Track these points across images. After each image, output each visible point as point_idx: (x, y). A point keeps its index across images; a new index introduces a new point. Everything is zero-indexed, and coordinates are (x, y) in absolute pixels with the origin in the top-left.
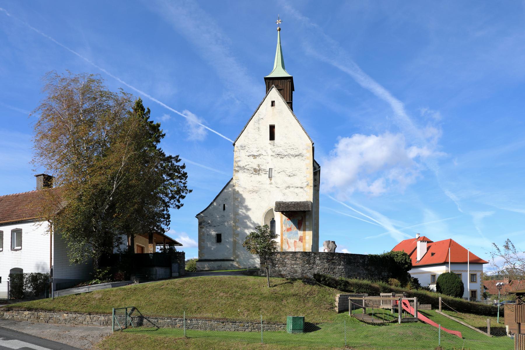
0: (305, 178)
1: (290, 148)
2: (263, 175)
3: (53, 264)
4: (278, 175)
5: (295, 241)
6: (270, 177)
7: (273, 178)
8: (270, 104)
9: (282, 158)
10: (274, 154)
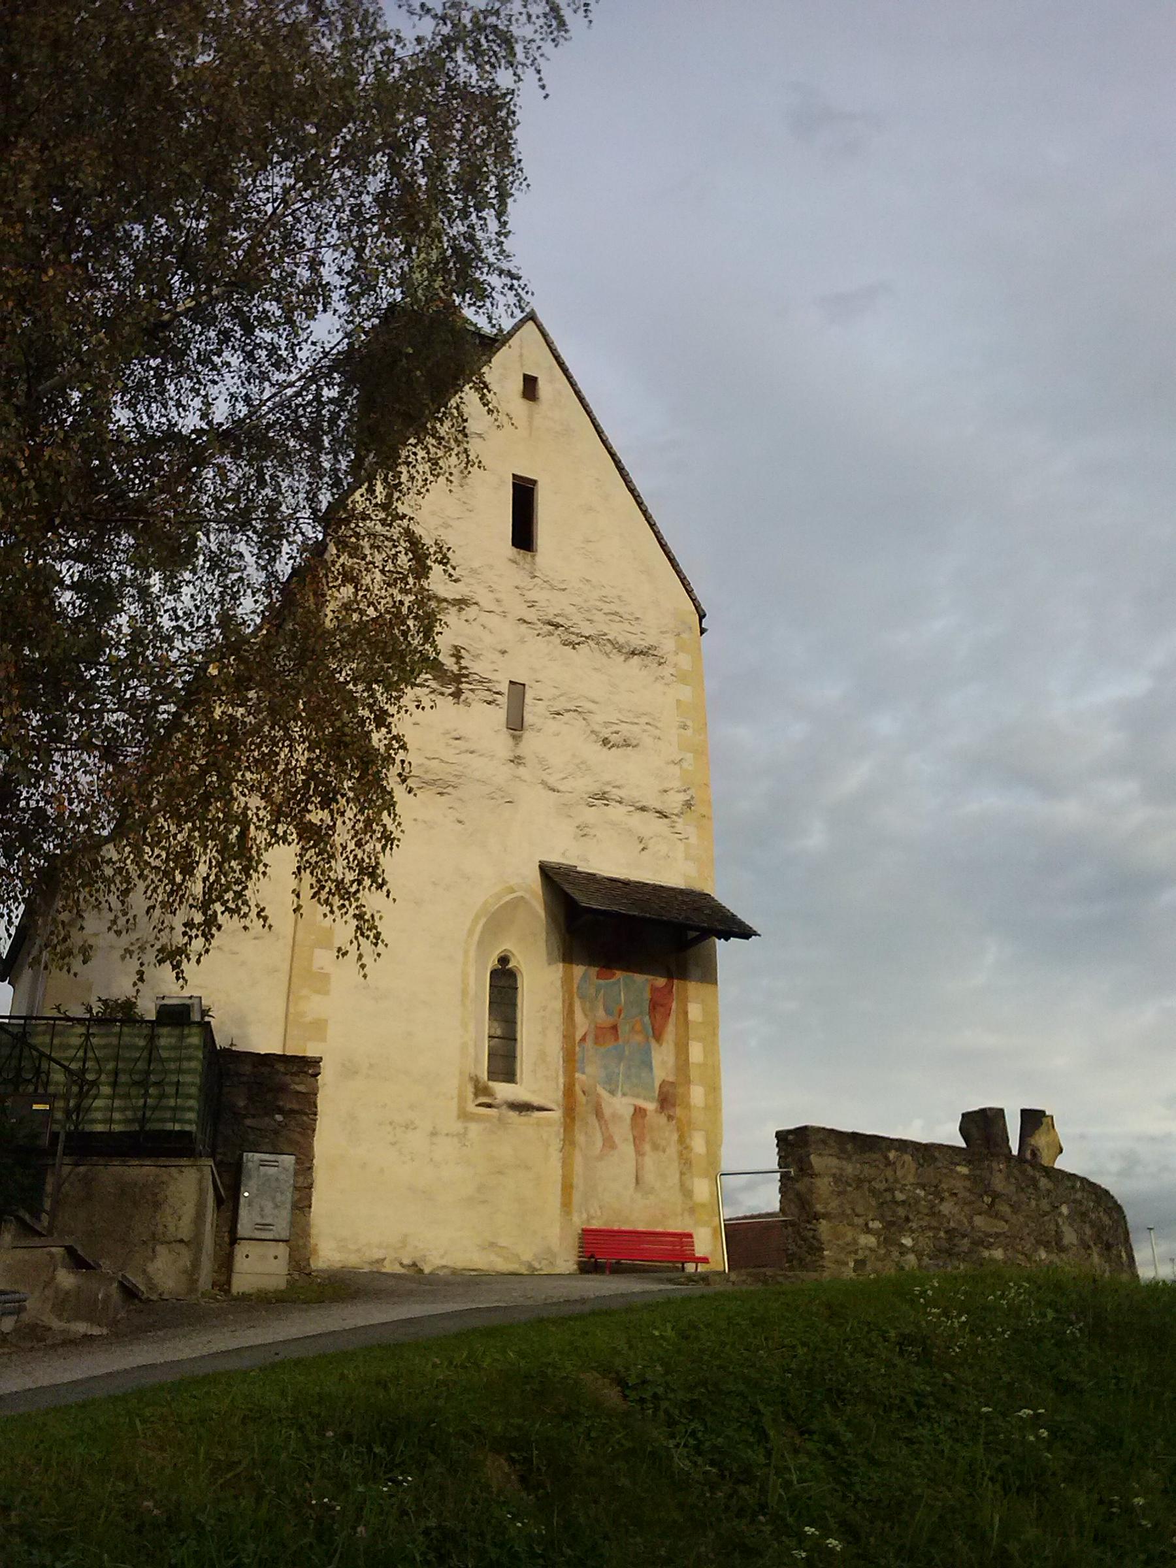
0: (676, 770)
1: (607, 608)
2: (479, 708)
3: (467, 1273)
4: (553, 725)
5: (639, 1112)
6: (516, 725)
7: (527, 735)
8: (519, 385)
10: (531, 615)
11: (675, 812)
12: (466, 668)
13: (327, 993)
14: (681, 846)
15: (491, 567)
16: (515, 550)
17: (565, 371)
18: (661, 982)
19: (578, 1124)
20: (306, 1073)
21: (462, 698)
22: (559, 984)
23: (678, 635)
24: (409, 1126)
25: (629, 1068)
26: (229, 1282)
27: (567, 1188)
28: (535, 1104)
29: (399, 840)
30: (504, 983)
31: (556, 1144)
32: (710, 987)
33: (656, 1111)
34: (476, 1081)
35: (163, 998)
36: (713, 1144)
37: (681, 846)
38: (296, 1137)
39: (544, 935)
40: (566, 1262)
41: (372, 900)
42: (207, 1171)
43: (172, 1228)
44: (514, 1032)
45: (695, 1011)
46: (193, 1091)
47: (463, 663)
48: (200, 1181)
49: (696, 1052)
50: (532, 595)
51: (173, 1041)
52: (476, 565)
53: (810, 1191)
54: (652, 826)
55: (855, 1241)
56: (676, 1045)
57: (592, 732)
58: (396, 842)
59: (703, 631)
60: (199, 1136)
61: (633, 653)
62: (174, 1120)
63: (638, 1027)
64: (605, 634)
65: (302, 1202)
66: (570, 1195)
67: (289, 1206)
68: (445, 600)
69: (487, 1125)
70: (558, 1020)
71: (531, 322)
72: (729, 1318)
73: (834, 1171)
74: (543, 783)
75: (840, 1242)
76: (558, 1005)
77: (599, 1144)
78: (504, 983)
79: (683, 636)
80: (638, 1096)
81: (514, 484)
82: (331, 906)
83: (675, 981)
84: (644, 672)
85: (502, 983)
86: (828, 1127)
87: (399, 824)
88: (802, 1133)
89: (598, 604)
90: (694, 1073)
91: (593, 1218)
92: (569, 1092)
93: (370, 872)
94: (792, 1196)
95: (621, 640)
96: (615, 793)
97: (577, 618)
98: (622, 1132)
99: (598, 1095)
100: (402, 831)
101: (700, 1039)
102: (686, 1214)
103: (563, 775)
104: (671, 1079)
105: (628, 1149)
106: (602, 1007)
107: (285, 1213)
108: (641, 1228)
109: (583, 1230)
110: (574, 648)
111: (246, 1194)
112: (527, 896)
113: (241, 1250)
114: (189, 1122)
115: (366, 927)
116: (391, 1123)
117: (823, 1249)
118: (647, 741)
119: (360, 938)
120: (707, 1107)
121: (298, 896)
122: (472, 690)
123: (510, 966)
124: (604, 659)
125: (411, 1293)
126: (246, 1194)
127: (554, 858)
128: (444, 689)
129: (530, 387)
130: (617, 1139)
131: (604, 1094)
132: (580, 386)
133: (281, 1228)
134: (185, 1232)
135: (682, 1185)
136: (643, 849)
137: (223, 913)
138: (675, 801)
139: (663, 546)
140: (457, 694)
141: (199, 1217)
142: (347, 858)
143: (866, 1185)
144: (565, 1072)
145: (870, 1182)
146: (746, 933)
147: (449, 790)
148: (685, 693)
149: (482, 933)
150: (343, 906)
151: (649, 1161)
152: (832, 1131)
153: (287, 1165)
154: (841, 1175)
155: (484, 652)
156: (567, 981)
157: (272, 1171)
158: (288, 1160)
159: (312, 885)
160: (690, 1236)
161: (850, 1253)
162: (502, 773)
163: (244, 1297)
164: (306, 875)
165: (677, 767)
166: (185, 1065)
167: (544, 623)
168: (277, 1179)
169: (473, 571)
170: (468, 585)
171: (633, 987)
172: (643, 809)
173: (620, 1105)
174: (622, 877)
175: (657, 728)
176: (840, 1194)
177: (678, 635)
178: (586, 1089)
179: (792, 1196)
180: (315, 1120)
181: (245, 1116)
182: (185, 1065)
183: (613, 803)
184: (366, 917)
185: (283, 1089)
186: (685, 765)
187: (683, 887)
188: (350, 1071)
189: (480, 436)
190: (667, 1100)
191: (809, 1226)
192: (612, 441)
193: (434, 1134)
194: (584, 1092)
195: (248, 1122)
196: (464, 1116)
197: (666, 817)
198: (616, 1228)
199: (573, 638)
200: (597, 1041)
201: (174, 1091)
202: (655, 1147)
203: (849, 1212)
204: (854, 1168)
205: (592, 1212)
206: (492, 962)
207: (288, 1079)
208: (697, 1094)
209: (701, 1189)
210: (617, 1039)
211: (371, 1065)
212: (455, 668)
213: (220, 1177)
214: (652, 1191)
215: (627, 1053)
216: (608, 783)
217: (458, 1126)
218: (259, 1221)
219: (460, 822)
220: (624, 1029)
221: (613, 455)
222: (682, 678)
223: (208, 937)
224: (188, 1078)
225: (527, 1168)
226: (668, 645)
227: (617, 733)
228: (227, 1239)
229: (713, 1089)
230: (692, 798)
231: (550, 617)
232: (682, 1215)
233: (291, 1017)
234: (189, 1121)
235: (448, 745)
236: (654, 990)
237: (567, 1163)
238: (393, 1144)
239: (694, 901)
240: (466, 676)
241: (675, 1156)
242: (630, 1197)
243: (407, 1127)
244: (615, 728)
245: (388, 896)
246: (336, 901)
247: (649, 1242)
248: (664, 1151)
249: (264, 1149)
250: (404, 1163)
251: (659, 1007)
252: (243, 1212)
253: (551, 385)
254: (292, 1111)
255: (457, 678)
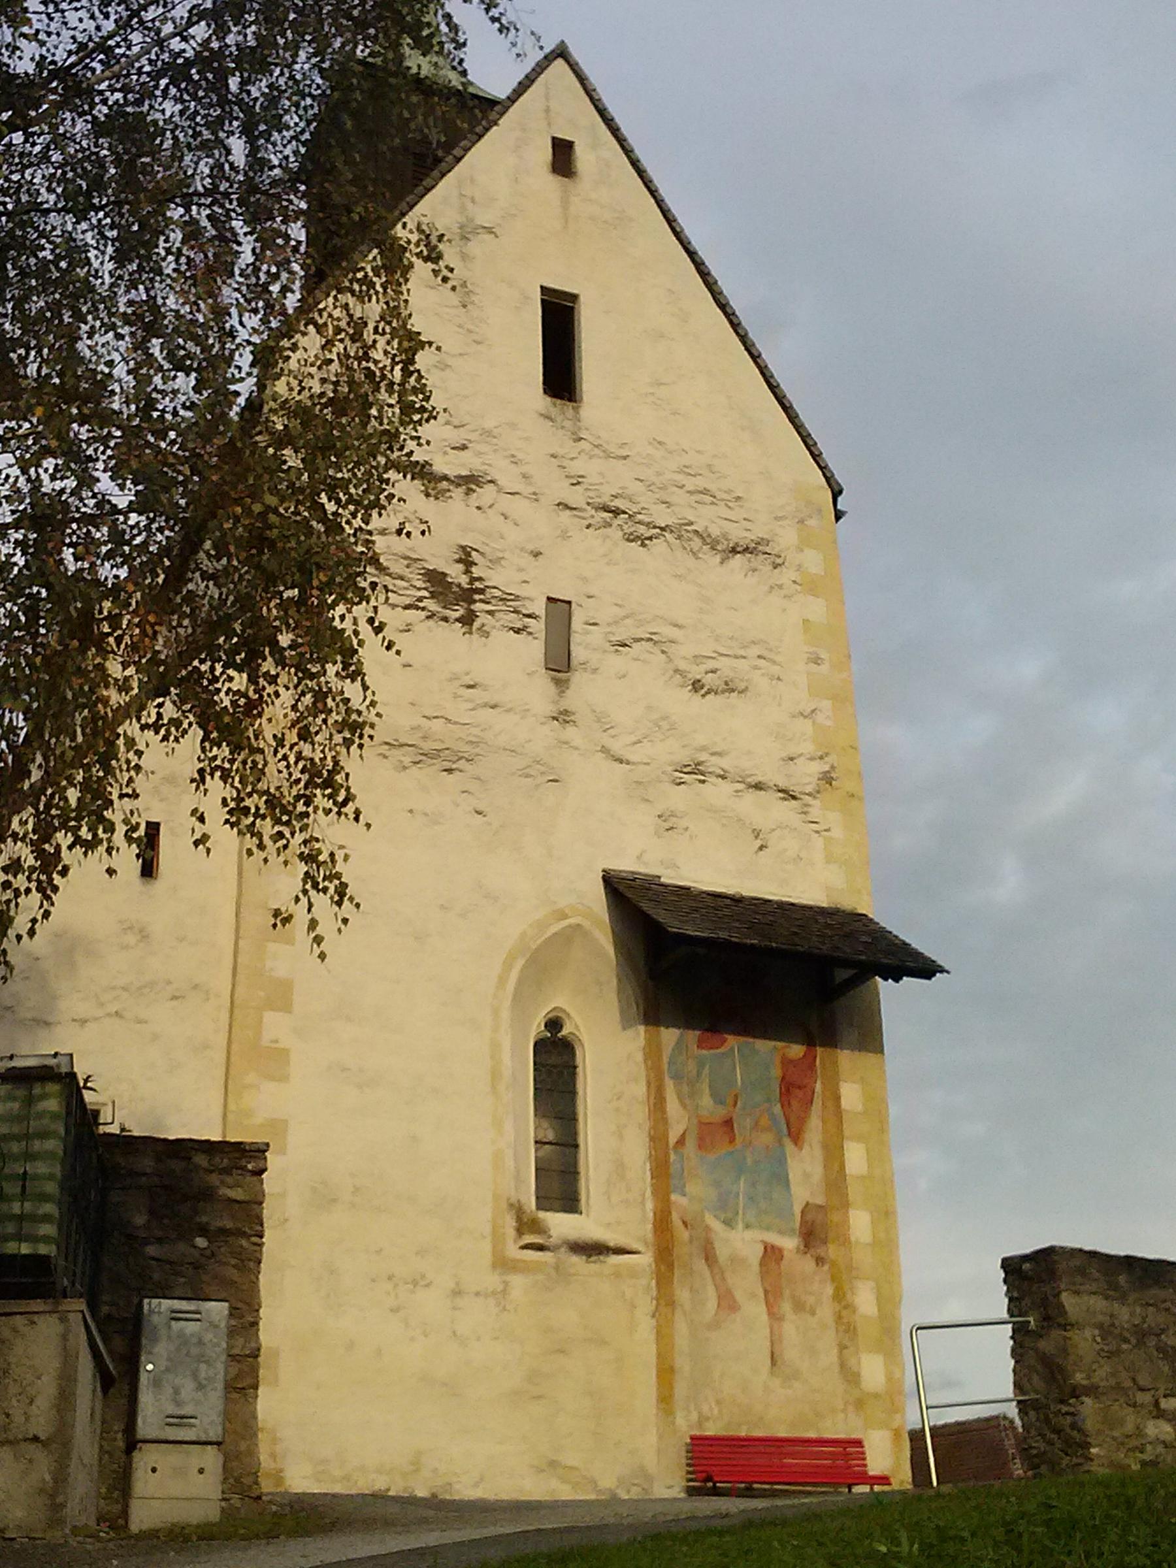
0: (806, 726)
1: (691, 483)
4: (616, 662)
5: (771, 1253)
6: (560, 663)
7: (577, 678)
9: (643, 541)
10: (576, 497)
11: (808, 789)
12: (480, 579)
13: (284, 1078)
14: (819, 842)
15: (513, 426)
16: (549, 399)
17: (615, 131)
18: (797, 1050)
19: (677, 1272)
20: (244, 1168)
21: (476, 625)
22: (639, 1057)
23: (801, 521)
24: (418, 1282)
25: (754, 1185)
26: (125, 1513)
27: (666, 1373)
28: (612, 1244)
29: (372, 726)
30: (555, 1060)
31: (646, 1305)
32: (869, 1059)
33: (798, 1249)
34: (518, 1210)
35: (11, 1057)
36: (888, 1302)
37: (819, 842)
38: (233, 1274)
39: (615, 981)
40: (668, 1484)
41: (330, 830)
42: (75, 1319)
43: (18, 1418)
44: (575, 1134)
45: (851, 1095)
46: (51, 1188)
47: (476, 571)
48: (64, 1337)
49: (855, 1157)
50: (577, 467)
51: (16, 1106)
52: (489, 424)
53: (1065, 1351)
54: (773, 812)
55: (1139, 1432)
56: (825, 1147)
57: (676, 671)
58: (367, 731)
59: (839, 516)
60: (62, 1263)
61: (734, 551)
62: (19, 1238)
63: (764, 1121)
64: (691, 524)
65: (243, 1375)
66: (671, 1387)
67: (220, 1386)
68: (445, 478)
69: (540, 1277)
70: (641, 1113)
71: (560, 62)
72: (1005, 1524)
73: (1100, 1318)
74: (604, 750)
75: (1116, 1434)
76: (640, 1089)
77: (712, 1304)
78: (555, 1060)
79: (811, 522)
80: (768, 1229)
81: (543, 301)
82: (260, 836)
83: (819, 1050)
84: (752, 580)
85: (554, 1060)
86: (1087, 1248)
87: (373, 704)
88: (1046, 1258)
89: (680, 478)
90: (854, 1191)
91: (708, 1419)
92: (662, 1223)
93: (325, 779)
94: (1032, 1362)
95: (715, 531)
96: (714, 764)
97: (646, 499)
98: (747, 1284)
99: (708, 1229)
100: (378, 715)
101: (859, 1138)
102: (851, 1408)
103: (634, 739)
104: (820, 1200)
105: (755, 1310)
106: (707, 1091)
107: (215, 1398)
108: (782, 1434)
109: (692, 1438)
110: (643, 545)
111: (150, 1367)
112: (586, 924)
113: (144, 1459)
114: (46, 1239)
115: (322, 874)
116: (390, 1278)
117: (1088, 1445)
118: (761, 682)
119: (313, 893)
120: (876, 1243)
121: (202, 819)
122: (490, 613)
123: (564, 1032)
124: (691, 562)
125: (424, 1521)
126: (150, 1367)
127: (625, 864)
128: (448, 613)
129: (563, 157)
130: (739, 1295)
131: (716, 1225)
132: (639, 153)
133: (209, 1423)
134: (41, 1421)
135: (843, 1365)
136: (761, 848)
137: (70, 848)
138: (807, 774)
139: (774, 388)
140: (468, 620)
141: (65, 1399)
142: (285, 757)
143: (1152, 1342)
144: (655, 1193)
145: (1158, 1335)
146: (926, 969)
147: (461, 764)
148: (816, 609)
149: (520, 982)
150: (280, 835)
151: (790, 1329)
152: (1093, 1254)
153: (216, 1318)
154: (1113, 1325)
155: (506, 555)
156: (652, 1052)
157: (191, 1327)
158: (217, 1310)
159: (224, 800)
160: (858, 1443)
161: (1133, 1449)
162: (540, 737)
163: (151, 1535)
164: (214, 784)
165: (809, 722)
166: (37, 1145)
167: (597, 509)
168: (200, 1342)
169: (488, 433)
170: (479, 454)
171: (757, 1058)
172: (758, 787)
173: (741, 1243)
174: (731, 891)
175: (774, 662)
176: (1111, 1355)
177: (801, 521)
178: (688, 1219)
179: (1032, 1362)
180: (261, 1245)
181: (146, 1242)
182: (37, 1145)
183: (713, 779)
184: (321, 858)
185: (208, 1195)
186: (820, 718)
187: (824, 905)
188: (323, 1198)
189: (490, 230)
190: (815, 1232)
191: (1065, 1409)
192: (689, 232)
193: (457, 1293)
194: (685, 1223)
195: (151, 1250)
196: (502, 1264)
197: (794, 798)
198: (743, 1434)
199: (642, 530)
200: (701, 1146)
201: (19, 1190)
202: (799, 1306)
203: (1128, 1383)
204: (1132, 1314)
205: (705, 1409)
206: (536, 1028)
207: (214, 1179)
208: (860, 1223)
209: (872, 1370)
210: (732, 1140)
211: (357, 1190)
212: (464, 580)
213: (105, 1341)
214: (796, 1375)
215: (749, 1161)
216: (703, 749)
217: (492, 1281)
218: (171, 1409)
219: (479, 813)
220: (743, 1125)
221: (691, 254)
222: (811, 586)
223: (47, 890)
224: (41, 1168)
225: (602, 1343)
226: (786, 538)
227: (713, 671)
228: (121, 1444)
229: (885, 1215)
230: (833, 767)
231: (606, 499)
232: (844, 1411)
233: (230, 1117)
234: (44, 1240)
235: (456, 696)
236: (786, 1062)
237: (663, 1336)
238: (395, 1310)
239: (842, 924)
240: (481, 591)
241: (830, 1320)
242: (767, 1385)
243: (415, 1283)
244: (711, 664)
245: (357, 819)
246: (267, 827)
247: (792, 1455)
248: (813, 1313)
249: (177, 1294)
250: (412, 1339)
251: (794, 1090)
252: (146, 1399)
253: (595, 152)
254: (223, 1231)
255: (468, 595)
